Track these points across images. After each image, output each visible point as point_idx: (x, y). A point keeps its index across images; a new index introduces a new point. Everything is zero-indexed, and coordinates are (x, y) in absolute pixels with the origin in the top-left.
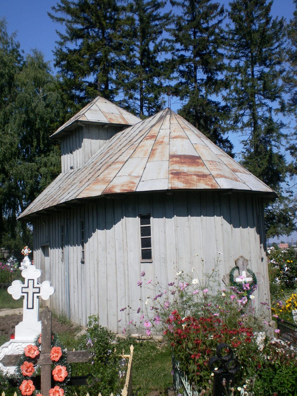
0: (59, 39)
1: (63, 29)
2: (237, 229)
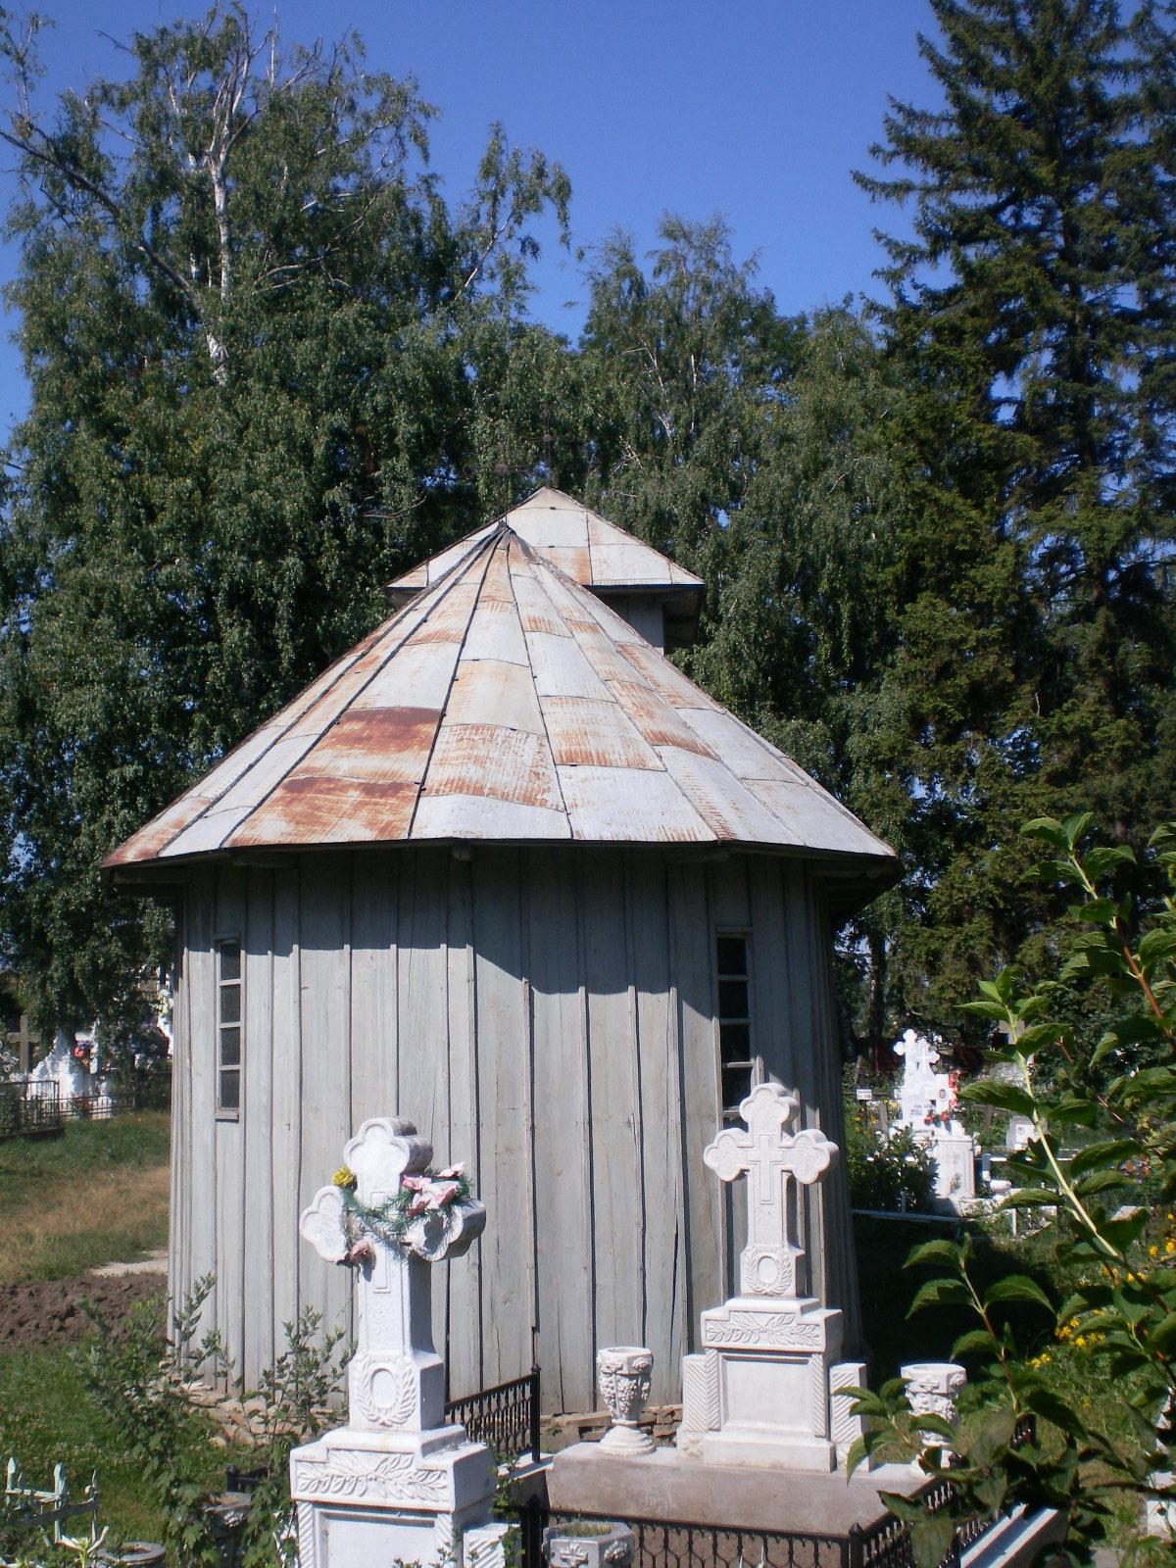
0: (886, 261)
1: (903, 221)
2: (556, 997)
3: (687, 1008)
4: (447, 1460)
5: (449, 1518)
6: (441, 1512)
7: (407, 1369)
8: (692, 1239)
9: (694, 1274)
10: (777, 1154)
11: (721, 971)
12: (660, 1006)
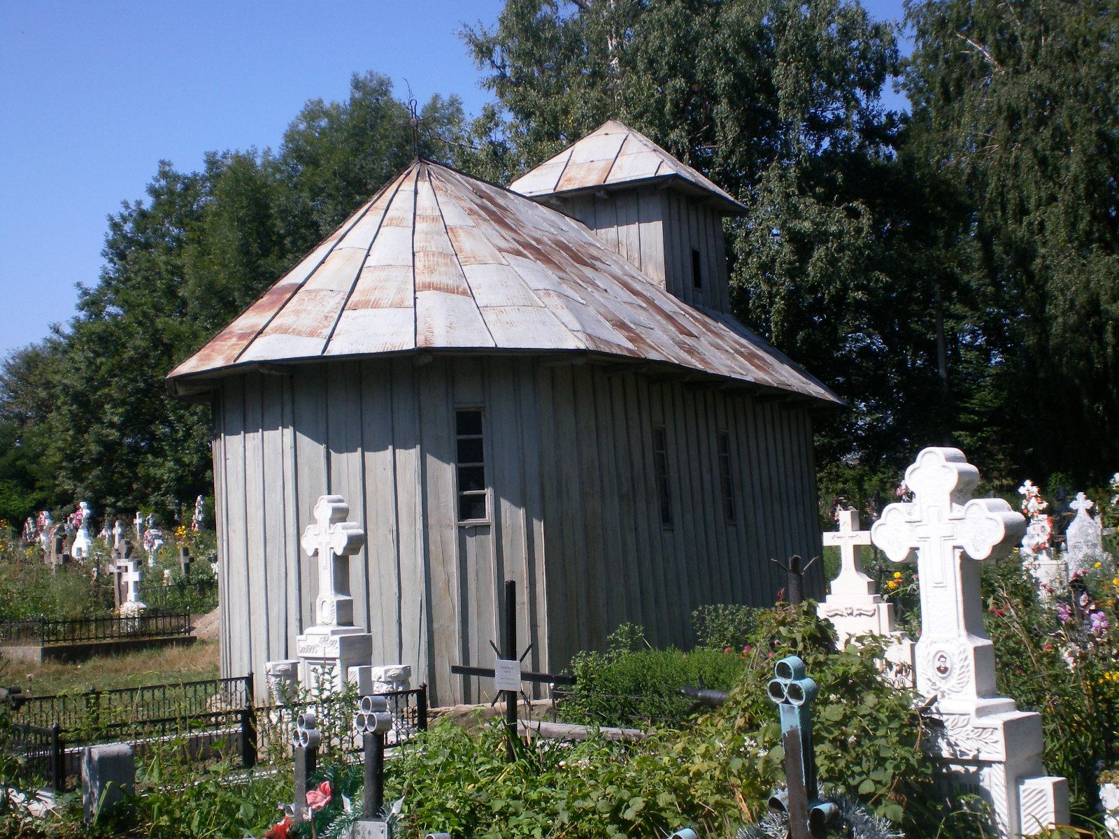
3: (430, 459)
4: (998, 720)
5: (1002, 767)
6: (994, 762)
7: (962, 648)
8: (434, 603)
9: (435, 626)
10: (947, 529)
11: (459, 433)
12: (409, 458)
